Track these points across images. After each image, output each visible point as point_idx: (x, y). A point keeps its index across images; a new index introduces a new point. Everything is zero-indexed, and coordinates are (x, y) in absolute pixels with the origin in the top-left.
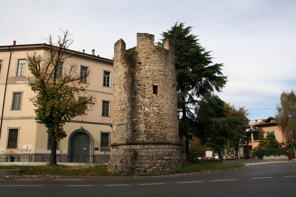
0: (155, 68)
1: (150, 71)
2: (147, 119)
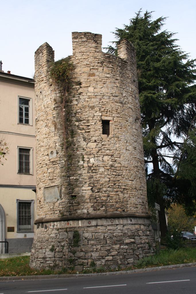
0: (104, 90)
1: (96, 96)
2: (94, 177)
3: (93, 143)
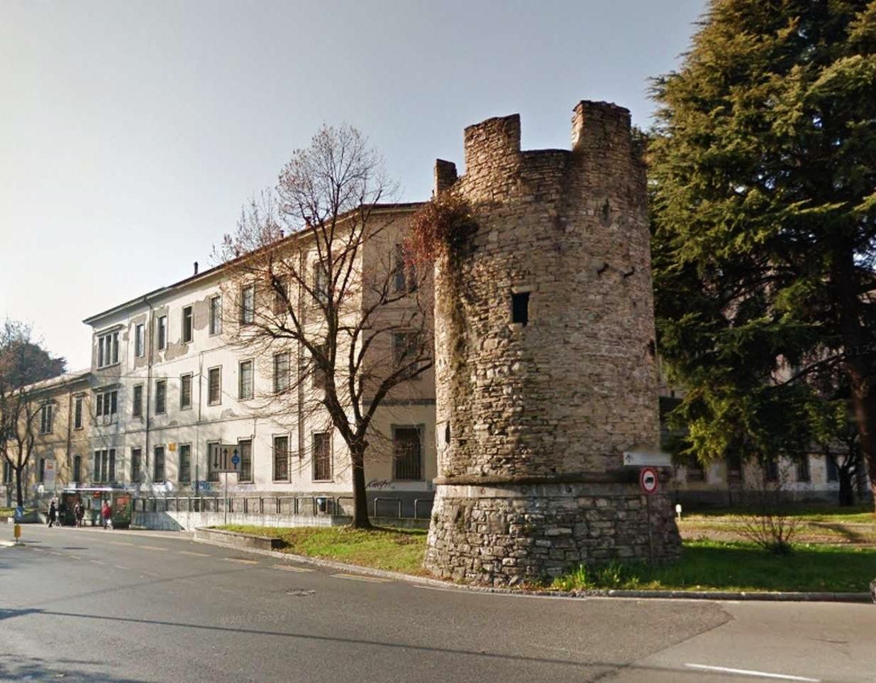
1: (502, 247)
2: (494, 405)
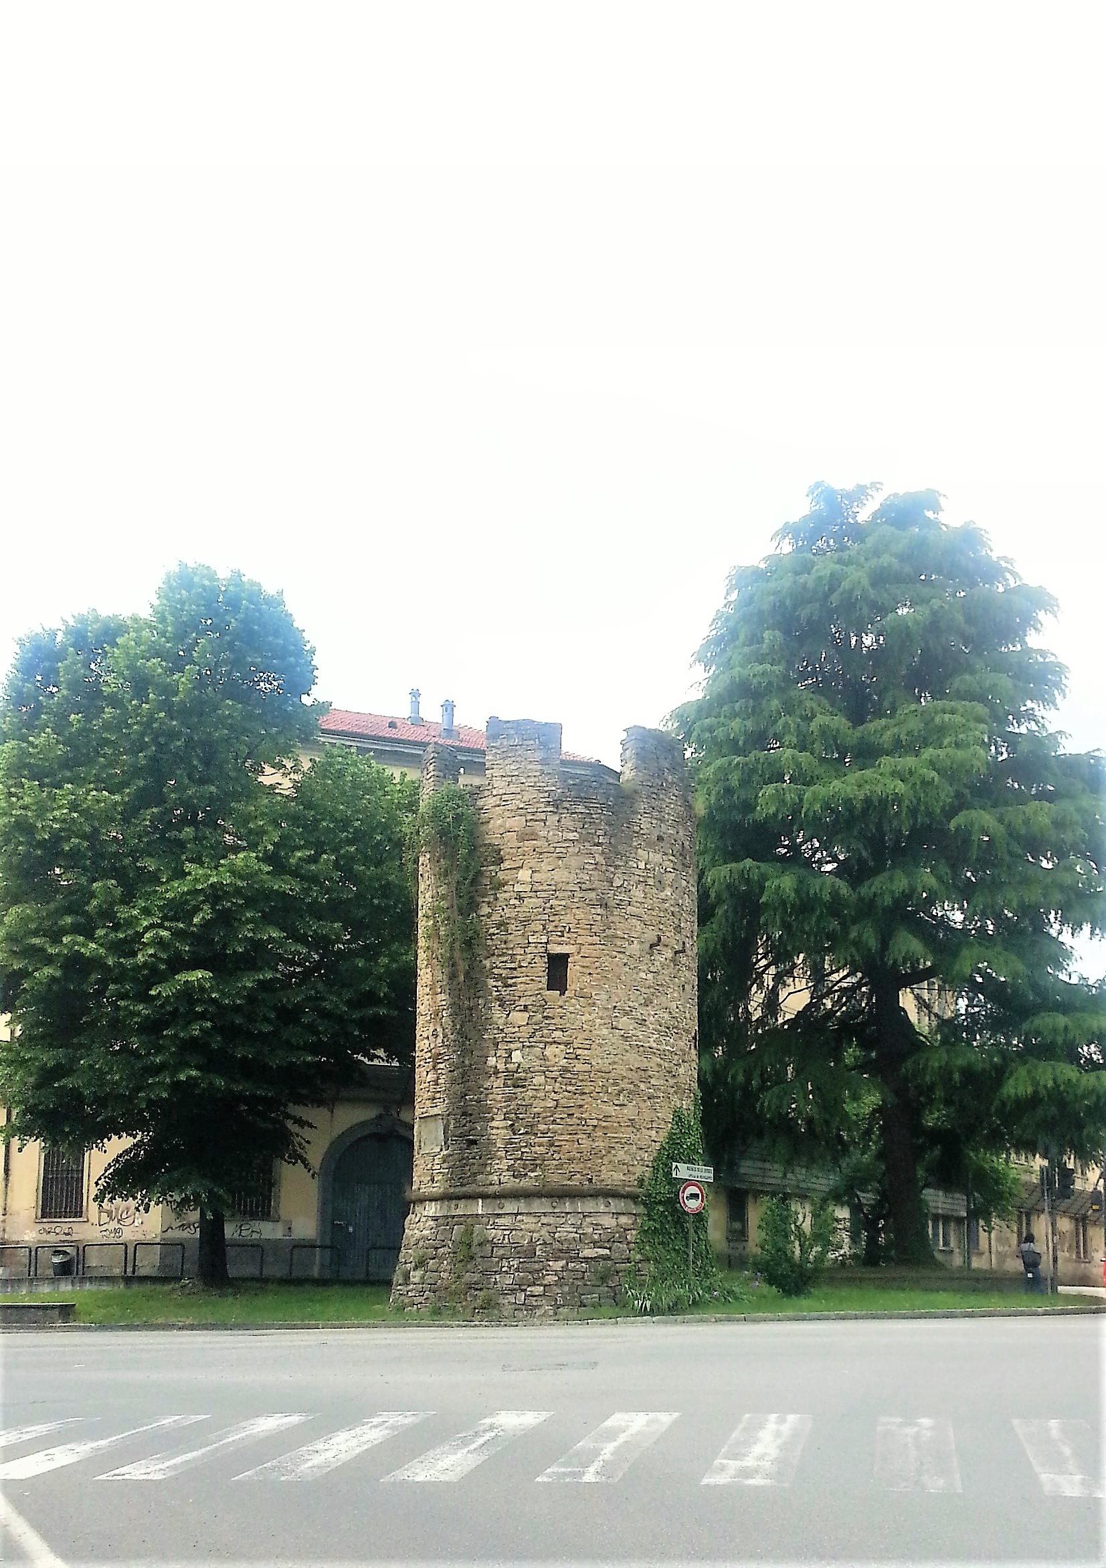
0: (560, 876)
3: (520, 1014)
